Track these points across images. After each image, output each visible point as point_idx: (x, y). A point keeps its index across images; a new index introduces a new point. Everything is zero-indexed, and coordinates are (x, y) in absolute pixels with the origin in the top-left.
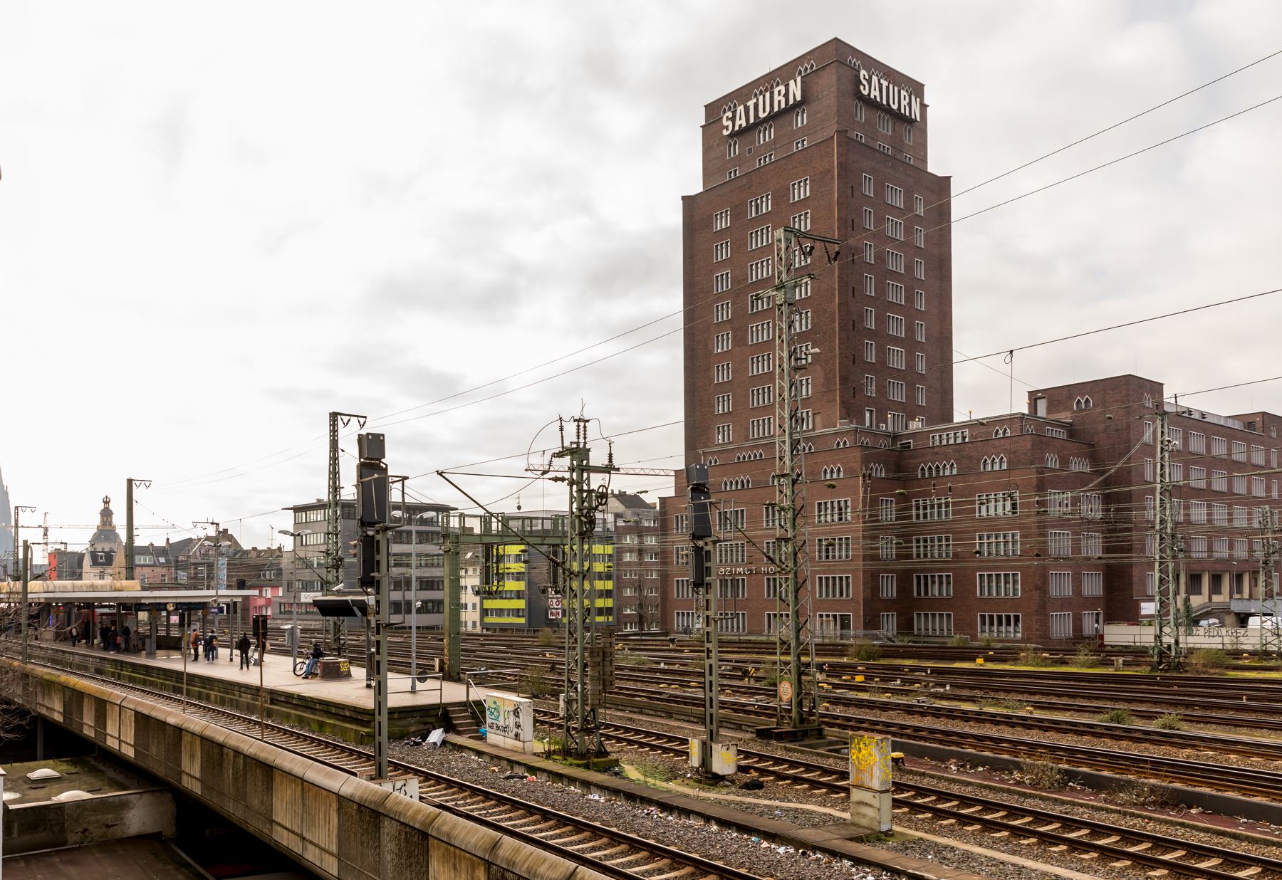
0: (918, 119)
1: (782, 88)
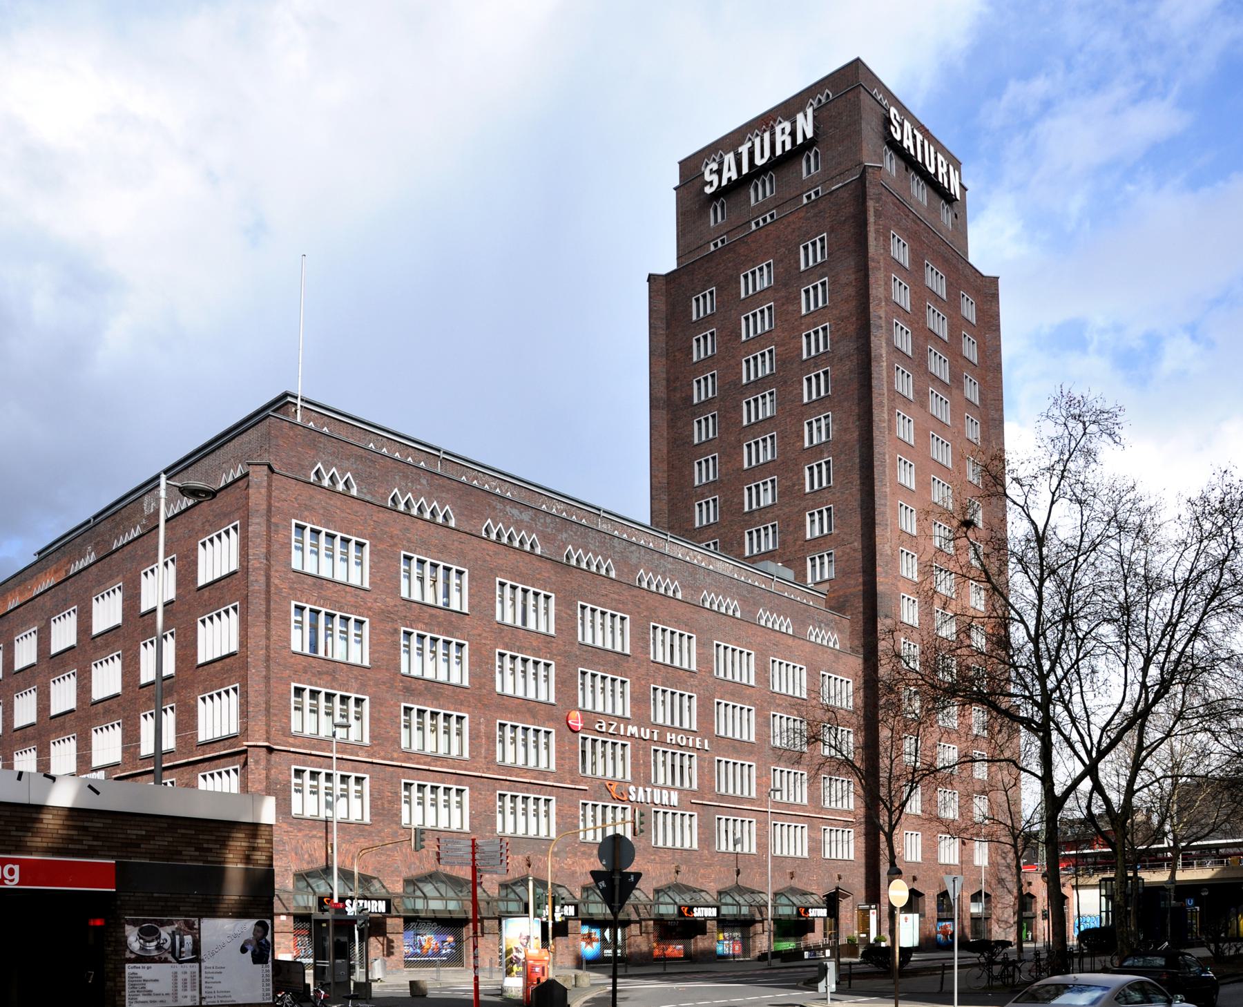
0: (958, 197)
1: (787, 126)
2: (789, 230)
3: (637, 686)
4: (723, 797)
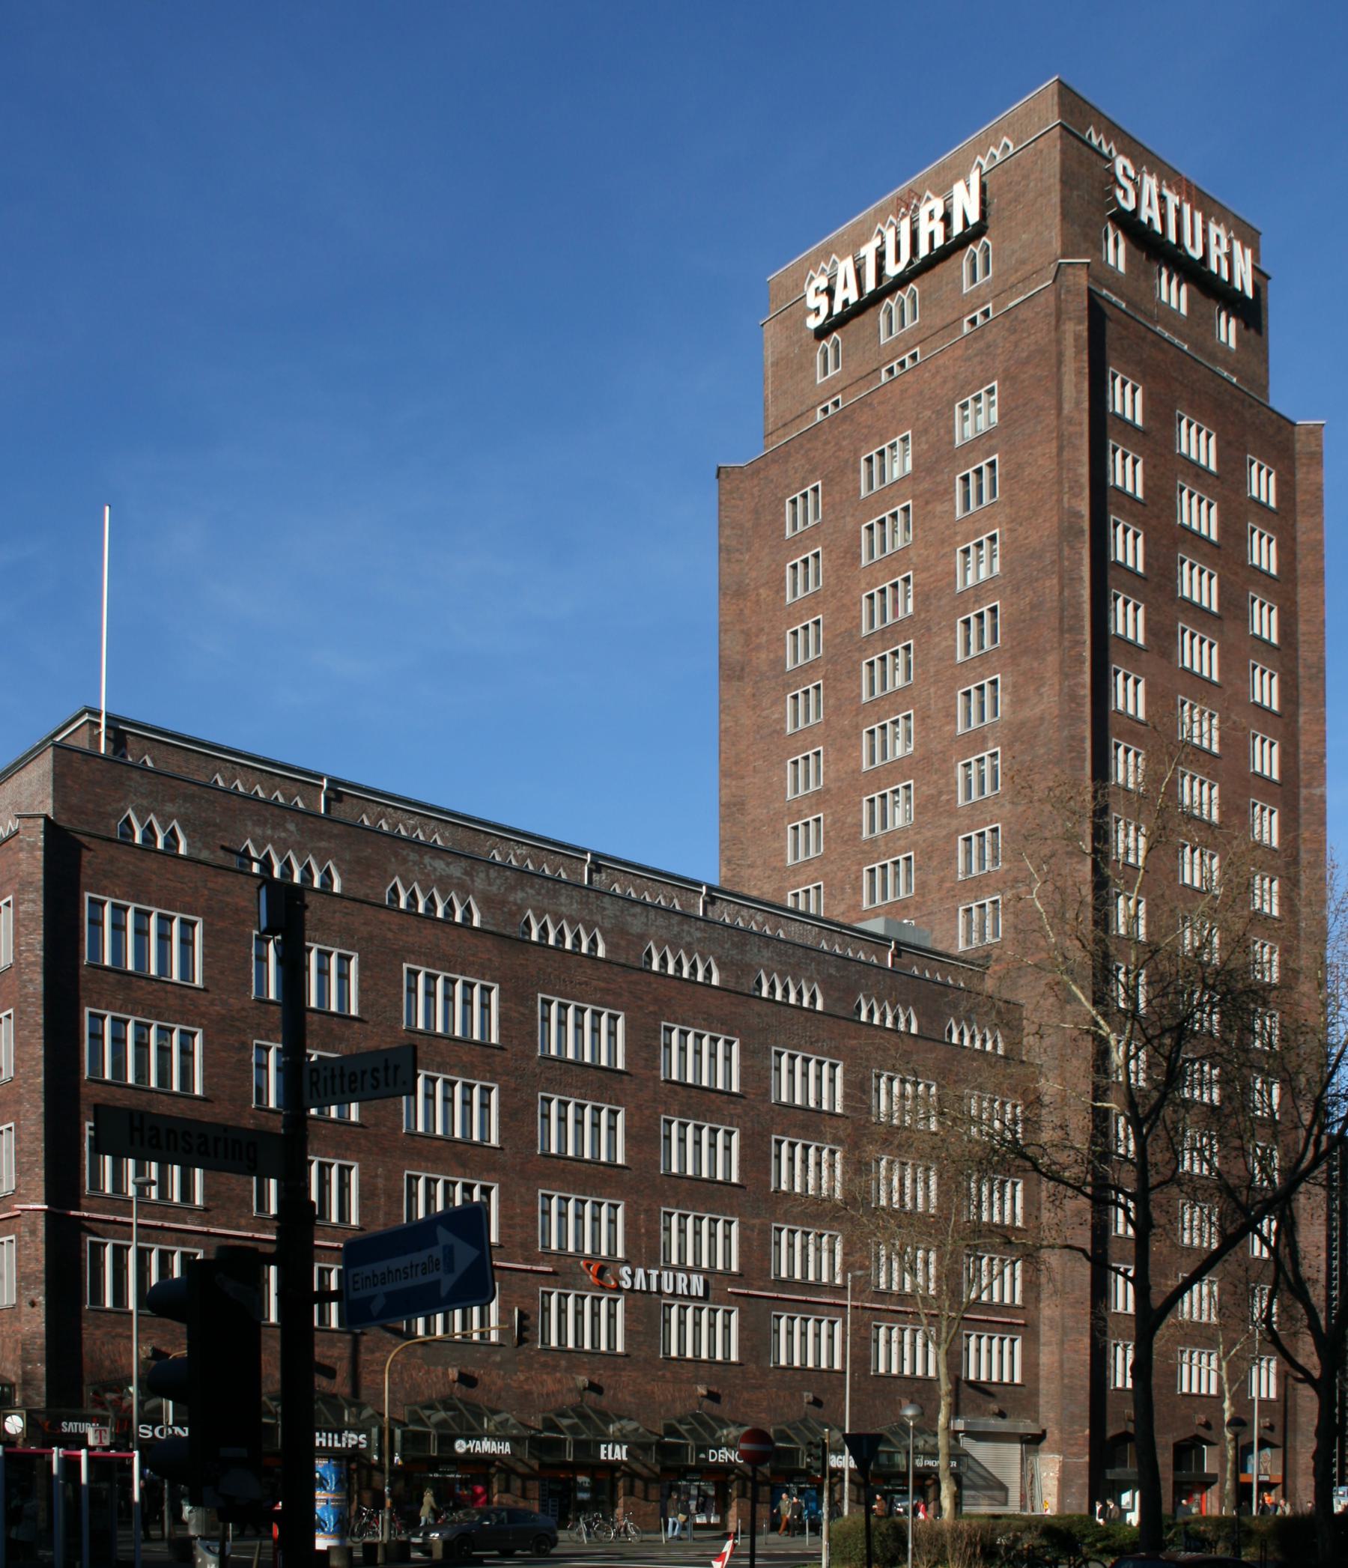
1: (938, 205)
2: (939, 380)
3: (636, 1118)
4: (789, 1284)
